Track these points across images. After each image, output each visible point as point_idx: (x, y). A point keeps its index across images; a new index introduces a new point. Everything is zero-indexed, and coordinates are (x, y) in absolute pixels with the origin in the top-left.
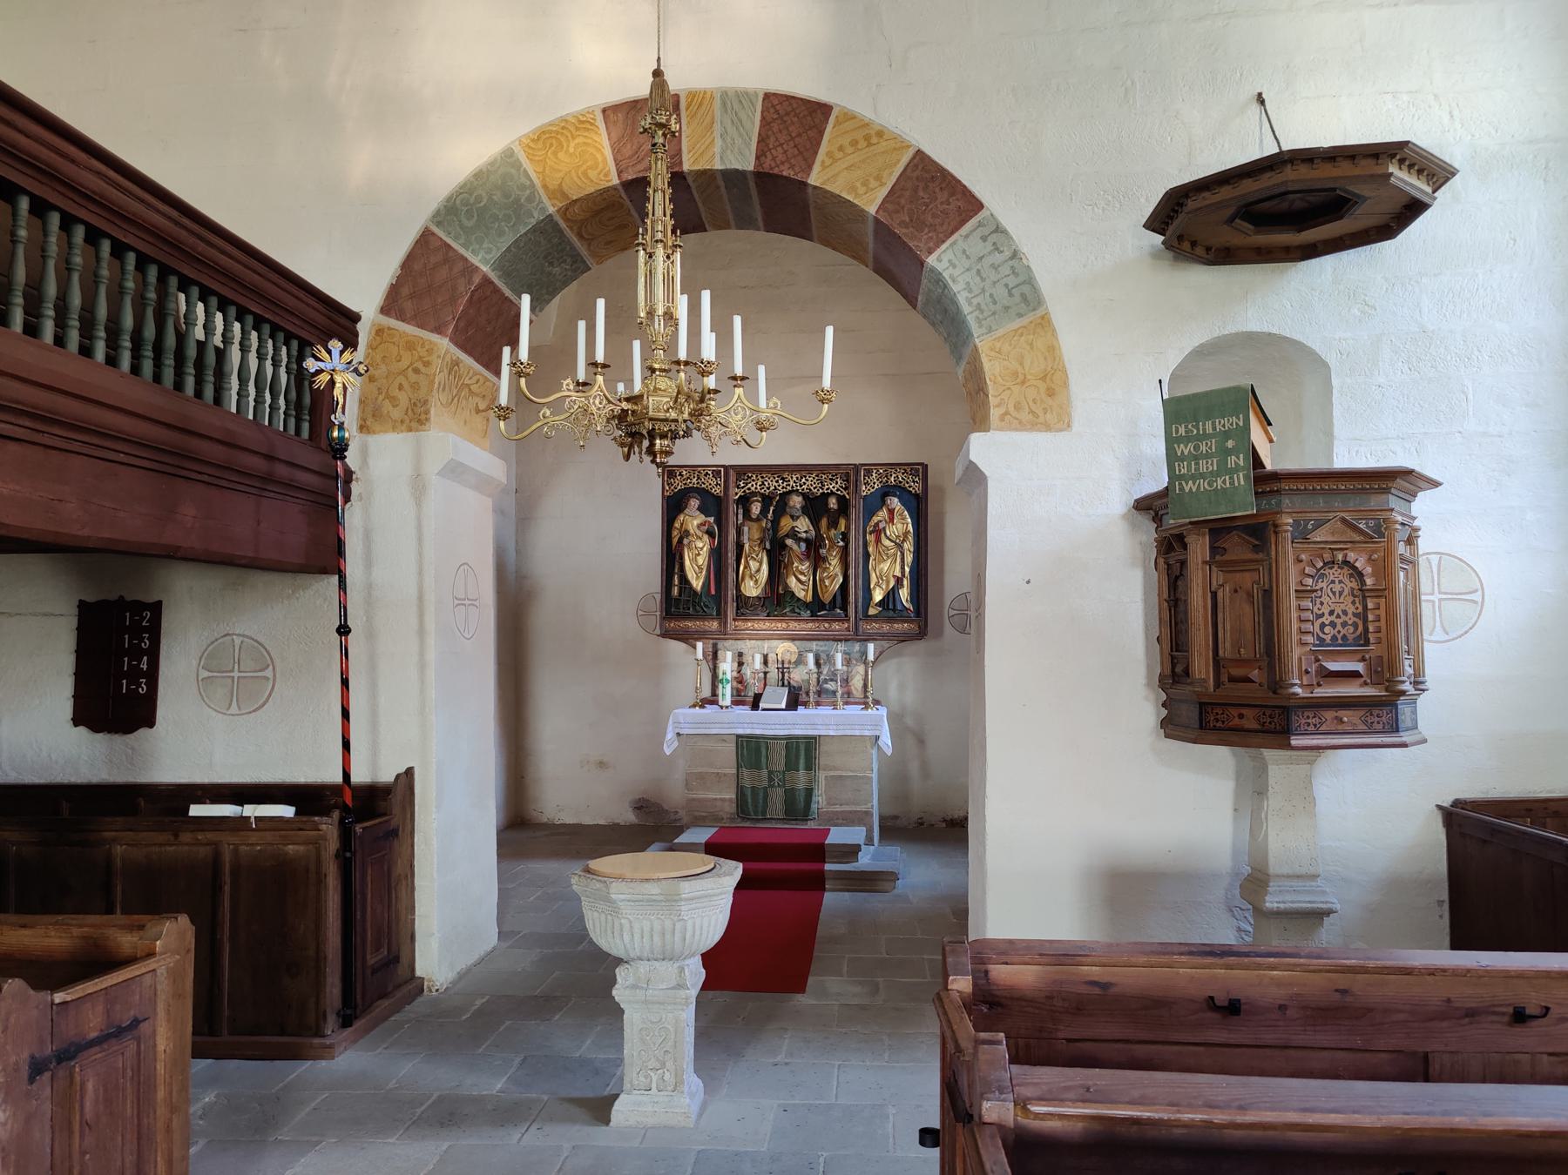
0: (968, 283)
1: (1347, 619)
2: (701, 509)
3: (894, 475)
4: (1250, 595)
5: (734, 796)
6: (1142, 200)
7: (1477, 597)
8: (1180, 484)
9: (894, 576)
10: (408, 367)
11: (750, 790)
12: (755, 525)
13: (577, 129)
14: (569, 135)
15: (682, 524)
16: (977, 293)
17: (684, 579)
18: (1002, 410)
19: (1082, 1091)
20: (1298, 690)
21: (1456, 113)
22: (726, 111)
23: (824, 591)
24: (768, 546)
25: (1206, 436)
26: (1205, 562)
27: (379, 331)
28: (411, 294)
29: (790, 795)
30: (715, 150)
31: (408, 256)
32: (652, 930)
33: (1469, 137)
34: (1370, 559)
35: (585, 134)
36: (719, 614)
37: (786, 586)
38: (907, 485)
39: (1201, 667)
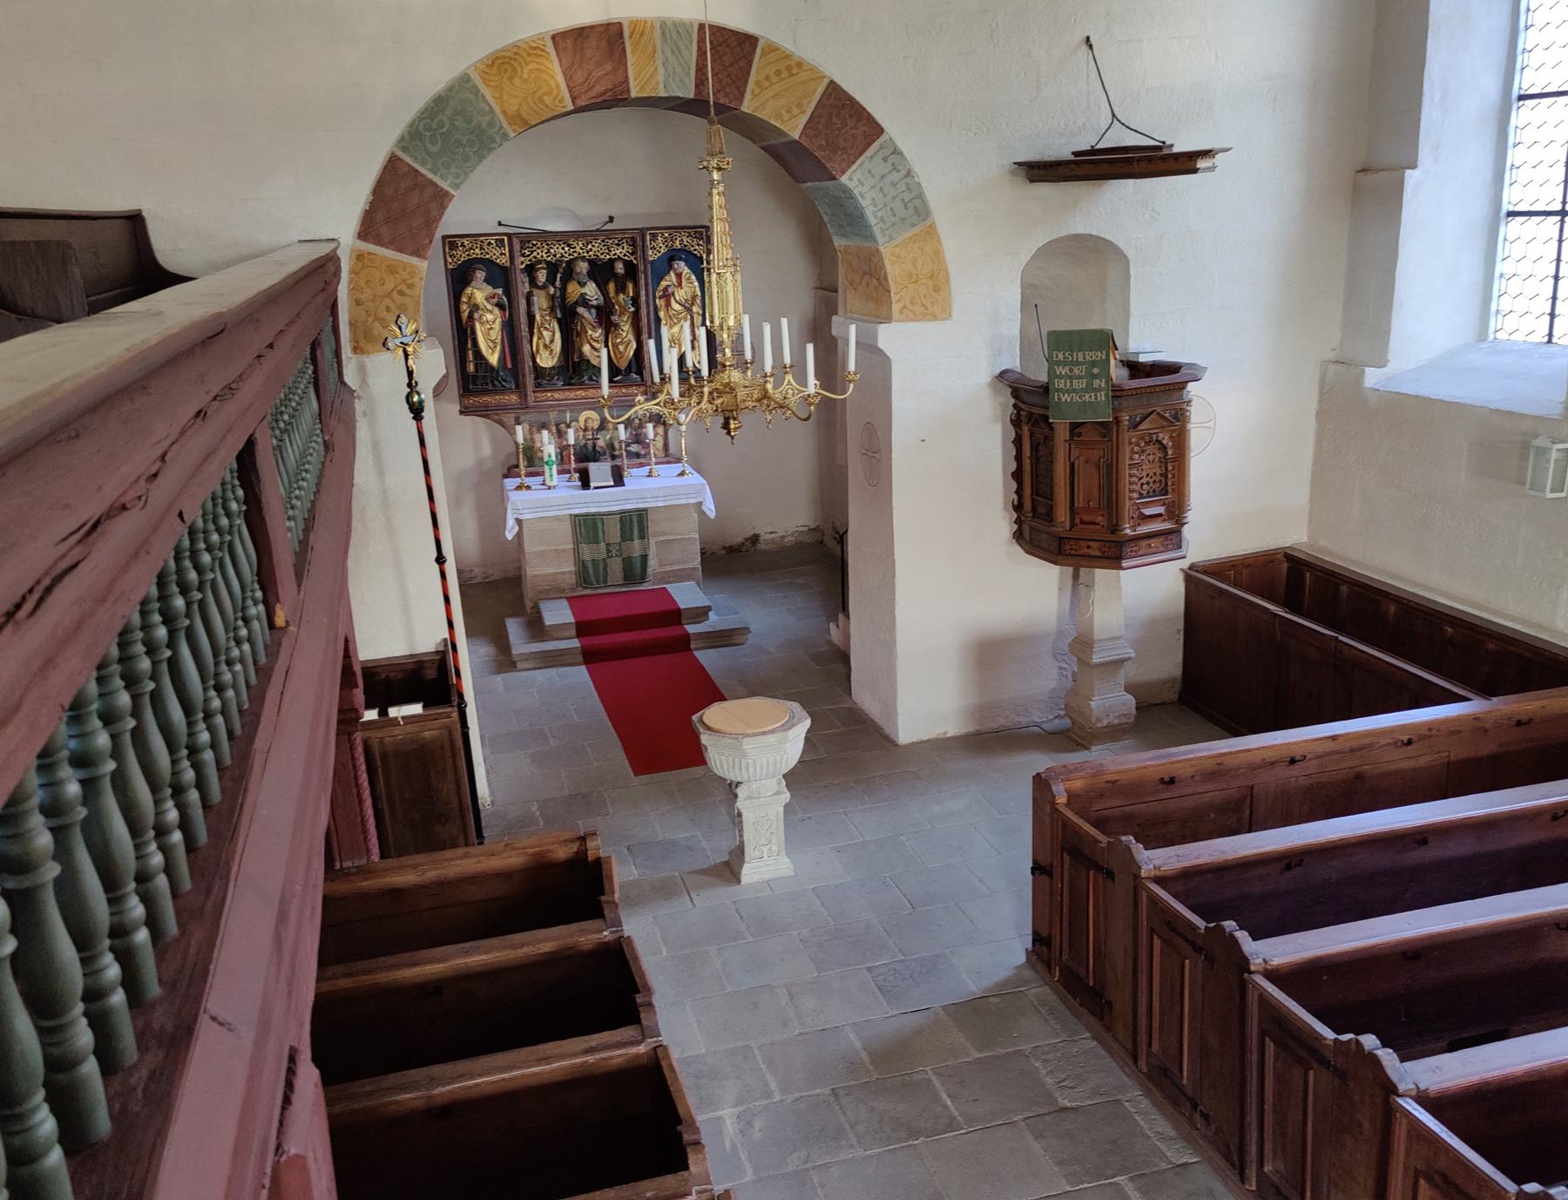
2: (488, 281)
7: (1211, 424)
8: (1058, 395)
10: (393, 290)
11: (590, 563)
12: (542, 293)
14: (522, 61)
15: (470, 298)
16: (881, 206)
17: (478, 355)
18: (900, 305)
20: (1128, 531)
22: (666, 41)
23: (619, 356)
24: (559, 316)
25: (1078, 363)
26: (1065, 441)
27: (360, 257)
28: (386, 219)
29: (628, 563)
30: (659, 78)
34: (1171, 437)
36: (517, 386)
37: (581, 354)
38: (692, 249)
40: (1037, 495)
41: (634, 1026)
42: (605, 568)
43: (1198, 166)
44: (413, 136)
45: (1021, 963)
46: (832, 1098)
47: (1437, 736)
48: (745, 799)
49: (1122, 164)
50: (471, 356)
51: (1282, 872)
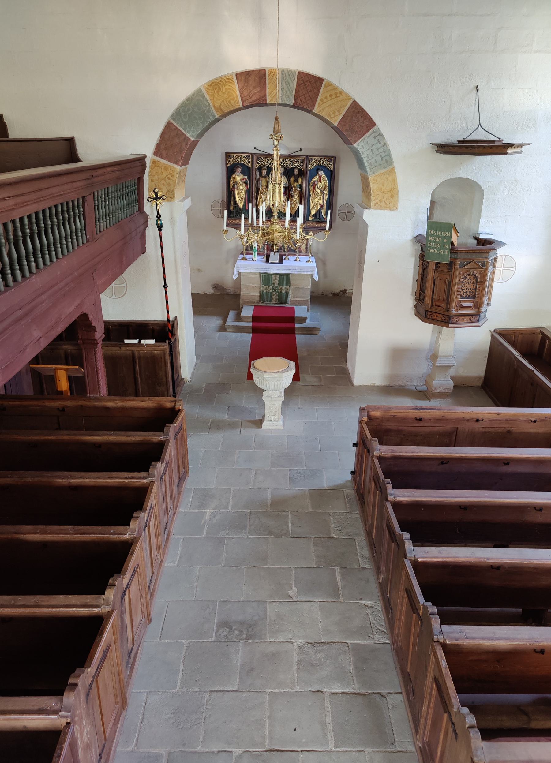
0: (368, 155)
1: (471, 290)
2: (242, 172)
3: (322, 161)
4: (445, 282)
5: (259, 294)
6: (432, 126)
7: (514, 269)
8: (429, 249)
9: (320, 205)
13: (226, 82)
14: (223, 84)
15: (234, 179)
17: (235, 203)
19: (391, 450)
20: (454, 312)
21: (542, 98)
22: (284, 79)
25: (438, 236)
26: (433, 269)
27: (154, 162)
28: (165, 148)
29: (280, 295)
31: (162, 132)
32: (275, 384)
33: (545, 107)
34: (480, 273)
35: (229, 85)
38: (327, 166)
39: (428, 301)
40: (422, 291)
41: (147, 473)
42: (271, 297)
43: (507, 152)
44: (178, 114)
45: (349, 479)
46: (249, 514)
47: (549, 421)
48: (266, 397)
49: (471, 148)
50: (232, 203)
51: (439, 465)
